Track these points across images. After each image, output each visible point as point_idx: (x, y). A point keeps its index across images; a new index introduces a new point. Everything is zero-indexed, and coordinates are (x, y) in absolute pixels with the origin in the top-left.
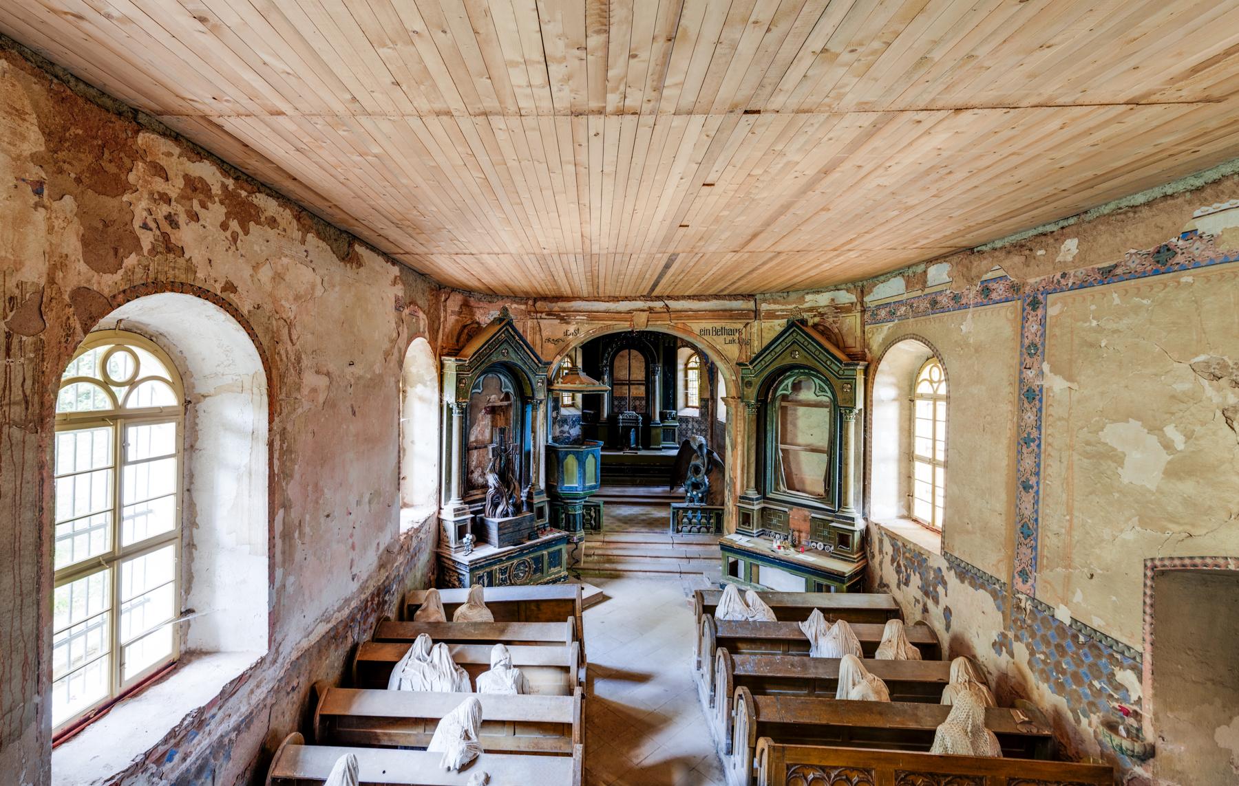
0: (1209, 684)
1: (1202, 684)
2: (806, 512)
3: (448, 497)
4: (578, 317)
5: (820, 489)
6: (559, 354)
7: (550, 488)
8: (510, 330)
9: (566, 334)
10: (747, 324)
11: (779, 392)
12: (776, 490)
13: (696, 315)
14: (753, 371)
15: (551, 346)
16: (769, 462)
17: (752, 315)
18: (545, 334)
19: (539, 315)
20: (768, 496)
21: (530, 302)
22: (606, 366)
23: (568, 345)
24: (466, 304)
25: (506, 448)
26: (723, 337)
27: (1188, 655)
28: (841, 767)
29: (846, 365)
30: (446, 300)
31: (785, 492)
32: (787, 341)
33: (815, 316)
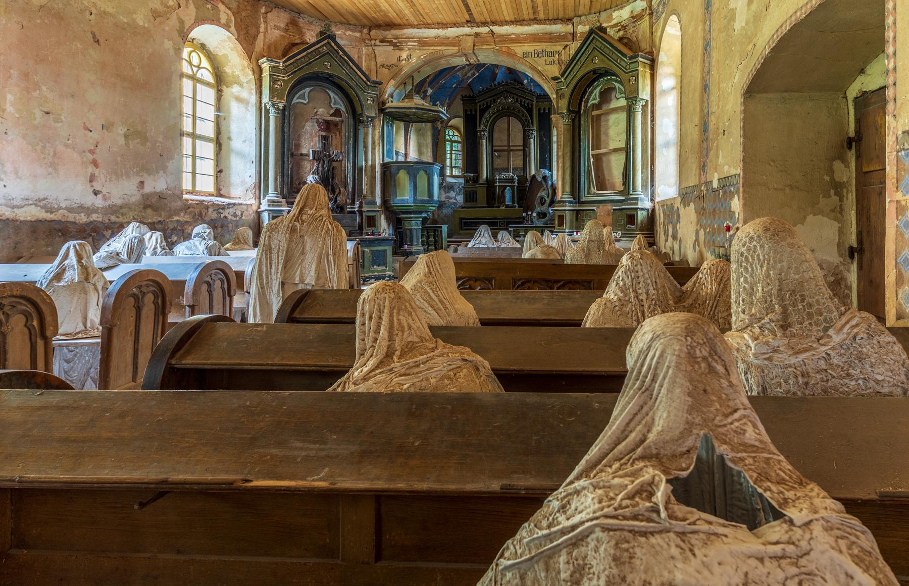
0: (787, 189)
1: (782, 190)
2: (610, 207)
4: (409, 44)
6: (393, 78)
7: (385, 201)
8: (333, 44)
9: (399, 60)
10: (566, 46)
11: (590, 103)
12: (589, 193)
13: (519, 39)
15: (386, 71)
16: (582, 168)
17: (570, 37)
18: (380, 60)
19: (373, 42)
21: (365, 31)
22: (483, 130)
23: (401, 70)
24: (293, 23)
25: (330, 154)
26: (545, 58)
27: (771, 166)
28: (465, 278)
29: (631, 58)
30: (266, 13)
31: (595, 193)
33: (619, 30)
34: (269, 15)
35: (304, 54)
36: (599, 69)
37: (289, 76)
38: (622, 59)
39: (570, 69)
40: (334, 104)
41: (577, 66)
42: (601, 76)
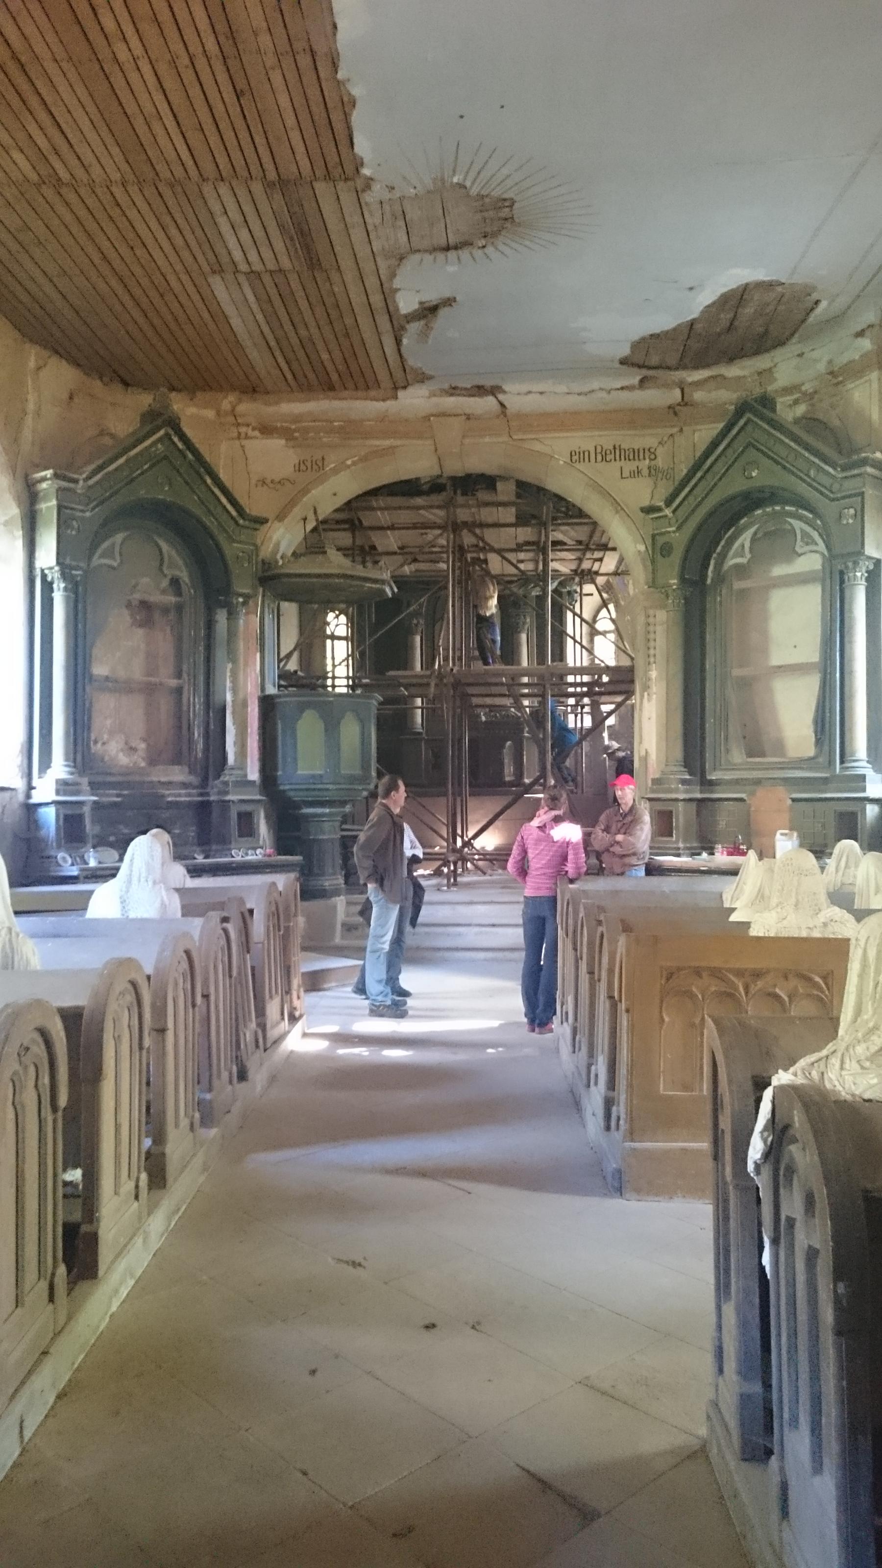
3: (46, 763)
5: (810, 751)
8: (176, 439)
11: (731, 562)
14: (673, 521)
19: (243, 430)
20: (709, 778)
26: (618, 464)
32: (735, 444)
34: (43, 374)
35: (121, 461)
36: (761, 490)
37: (93, 509)
38: (819, 469)
39: (687, 490)
40: (169, 567)
41: (691, 499)
42: (759, 503)
